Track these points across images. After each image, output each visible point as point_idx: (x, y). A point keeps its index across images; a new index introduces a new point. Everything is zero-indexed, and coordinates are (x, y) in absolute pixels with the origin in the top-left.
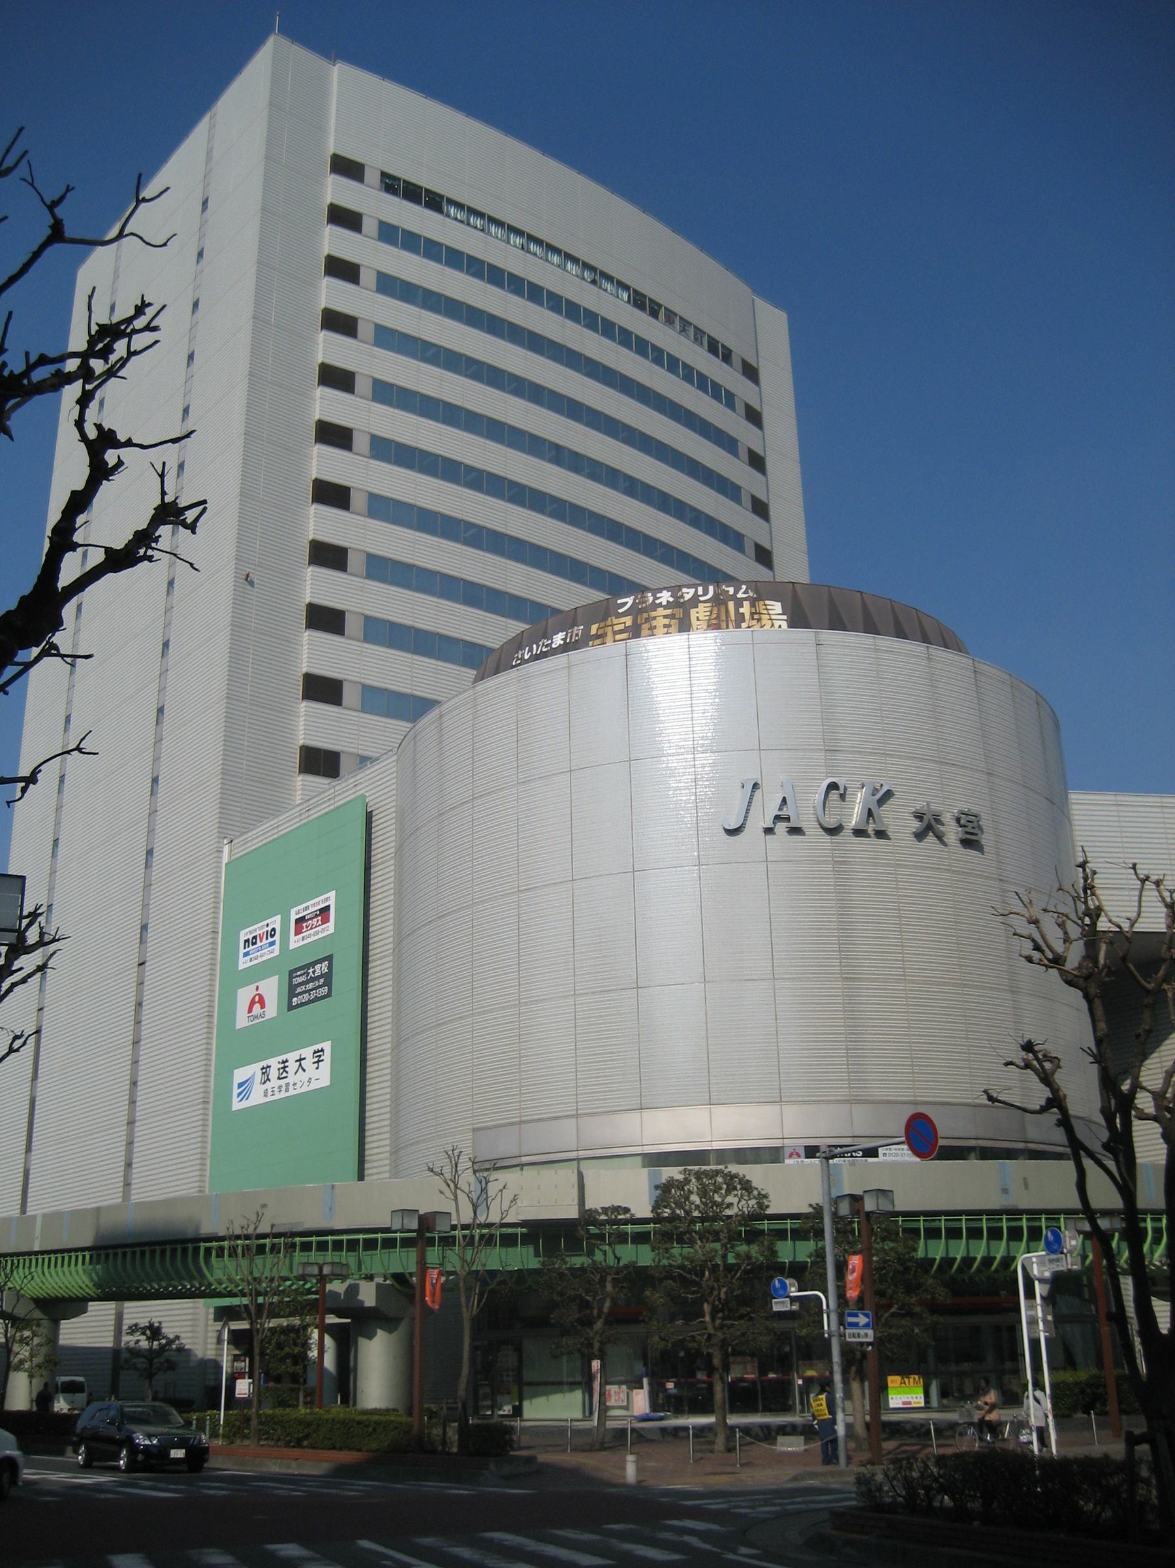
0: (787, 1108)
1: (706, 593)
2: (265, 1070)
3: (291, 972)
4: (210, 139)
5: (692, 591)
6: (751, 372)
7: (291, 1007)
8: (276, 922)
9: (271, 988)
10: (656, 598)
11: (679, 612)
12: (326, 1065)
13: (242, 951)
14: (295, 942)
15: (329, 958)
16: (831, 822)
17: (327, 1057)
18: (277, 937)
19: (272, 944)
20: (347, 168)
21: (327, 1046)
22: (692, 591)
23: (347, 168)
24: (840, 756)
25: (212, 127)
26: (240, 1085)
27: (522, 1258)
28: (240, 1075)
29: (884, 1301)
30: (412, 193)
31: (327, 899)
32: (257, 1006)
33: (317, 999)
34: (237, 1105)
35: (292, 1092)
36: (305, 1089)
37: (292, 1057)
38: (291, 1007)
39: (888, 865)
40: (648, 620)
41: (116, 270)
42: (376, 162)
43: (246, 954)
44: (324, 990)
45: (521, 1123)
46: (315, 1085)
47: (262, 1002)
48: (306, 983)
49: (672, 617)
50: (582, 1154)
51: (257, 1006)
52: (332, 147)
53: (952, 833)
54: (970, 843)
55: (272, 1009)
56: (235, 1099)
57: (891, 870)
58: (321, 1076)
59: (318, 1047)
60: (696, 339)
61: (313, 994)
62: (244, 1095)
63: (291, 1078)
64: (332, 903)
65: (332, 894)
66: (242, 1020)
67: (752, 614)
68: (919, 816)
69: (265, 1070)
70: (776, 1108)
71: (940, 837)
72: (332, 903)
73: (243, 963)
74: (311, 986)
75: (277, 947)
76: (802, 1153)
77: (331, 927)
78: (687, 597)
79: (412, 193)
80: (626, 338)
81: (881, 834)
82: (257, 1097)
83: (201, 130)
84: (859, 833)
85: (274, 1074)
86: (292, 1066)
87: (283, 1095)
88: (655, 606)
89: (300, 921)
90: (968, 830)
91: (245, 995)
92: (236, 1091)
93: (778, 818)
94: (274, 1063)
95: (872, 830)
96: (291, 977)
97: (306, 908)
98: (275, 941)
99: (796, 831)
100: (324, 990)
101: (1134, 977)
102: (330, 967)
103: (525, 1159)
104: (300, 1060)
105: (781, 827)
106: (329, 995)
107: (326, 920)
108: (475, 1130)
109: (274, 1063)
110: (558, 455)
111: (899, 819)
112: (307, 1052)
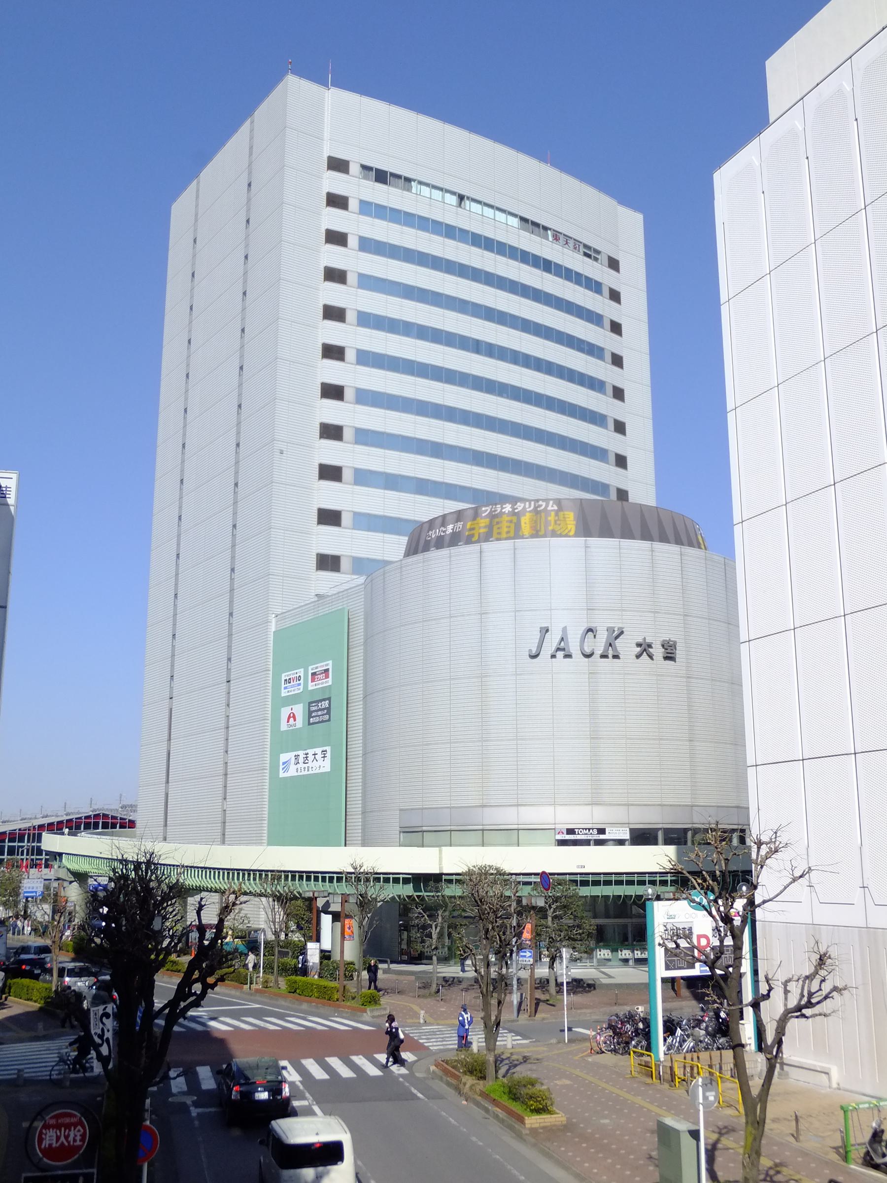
0: (558, 808)
1: (530, 506)
2: (297, 757)
3: (310, 703)
4: (252, 130)
5: (522, 505)
6: (614, 264)
7: (309, 724)
8: (301, 672)
9: (299, 710)
10: (502, 508)
11: (515, 519)
12: (328, 760)
13: (283, 686)
14: (311, 686)
15: (329, 699)
16: (588, 651)
17: (328, 755)
18: (302, 681)
19: (299, 685)
20: (338, 165)
21: (328, 749)
22: (522, 505)
23: (338, 165)
24: (597, 612)
25: (252, 122)
26: (284, 763)
27: (408, 890)
28: (284, 757)
29: (501, 954)
30: (381, 177)
31: (327, 665)
32: (292, 719)
33: (323, 721)
34: (282, 775)
35: (310, 772)
36: (317, 771)
37: (311, 752)
38: (309, 724)
39: (620, 674)
40: (498, 523)
41: (196, 215)
42: (355, 158)
43: (285, 688)
44: (327, 717)
45: (422, 809)
46: (322, 770)
47: (294, 717)
48: (319, 710)
49: (511, 522)
50: (453, 828)
51: (292, 719)
52: (328, 150)
53: (658, 652)
54: (670, 657)
55: (300, 723)
56: (281, 771)
57: (622, 676)
58: (325, 766)
59: (324, 748)
60: (575, 248)
61: (321, 718)
62: (286, 770)
63: (310, 764)
64: (330, 667)
65: (330, 662)
66: (284, 727)
67: (555, 521)
68: (639, 645)
69: (297, 757)
70: (552, 808)
71: (651, 657)
72: (330, 667)
73: (284, 693)
74: (320, 713)
75: (301, 687)
76: (565, 832)
77: (330, 681)
78: (520, 509)
79: (381, 177)
80: (525, 257)
81: (616, 657)
82: (292, 772)
83: (245, 127)
84: (604, 656)
85: (301, 760)
86: (311, 757)
87: (306, 773)
88: (502, 513)
89: (314, 674)
90: (669, 651)
91: (285, 712)
92: (281, 767)
93: (558, 649)
94: (301, 754)
95: (611, 653)
96: (309, 707)
97: (317, 668)
98: (301, 682)
99: (568, 656)
100: (327, 717)
101: (45, 1176)
102: (330, 705)
103: (424, 828)
104: (315, 754)
105: (560, 654)
106: (329, 720)
107: (327, 677)
108: (401, 810)
109: (301, 754)
110: (437, 450)
111: (627, 647)
112: (318, 751)
